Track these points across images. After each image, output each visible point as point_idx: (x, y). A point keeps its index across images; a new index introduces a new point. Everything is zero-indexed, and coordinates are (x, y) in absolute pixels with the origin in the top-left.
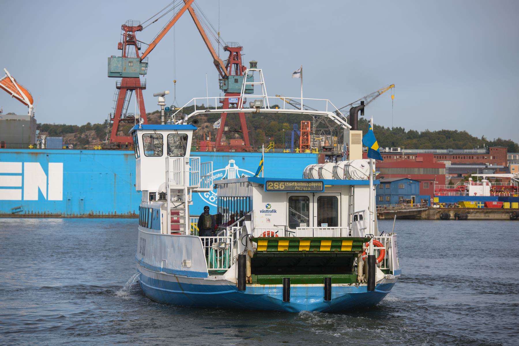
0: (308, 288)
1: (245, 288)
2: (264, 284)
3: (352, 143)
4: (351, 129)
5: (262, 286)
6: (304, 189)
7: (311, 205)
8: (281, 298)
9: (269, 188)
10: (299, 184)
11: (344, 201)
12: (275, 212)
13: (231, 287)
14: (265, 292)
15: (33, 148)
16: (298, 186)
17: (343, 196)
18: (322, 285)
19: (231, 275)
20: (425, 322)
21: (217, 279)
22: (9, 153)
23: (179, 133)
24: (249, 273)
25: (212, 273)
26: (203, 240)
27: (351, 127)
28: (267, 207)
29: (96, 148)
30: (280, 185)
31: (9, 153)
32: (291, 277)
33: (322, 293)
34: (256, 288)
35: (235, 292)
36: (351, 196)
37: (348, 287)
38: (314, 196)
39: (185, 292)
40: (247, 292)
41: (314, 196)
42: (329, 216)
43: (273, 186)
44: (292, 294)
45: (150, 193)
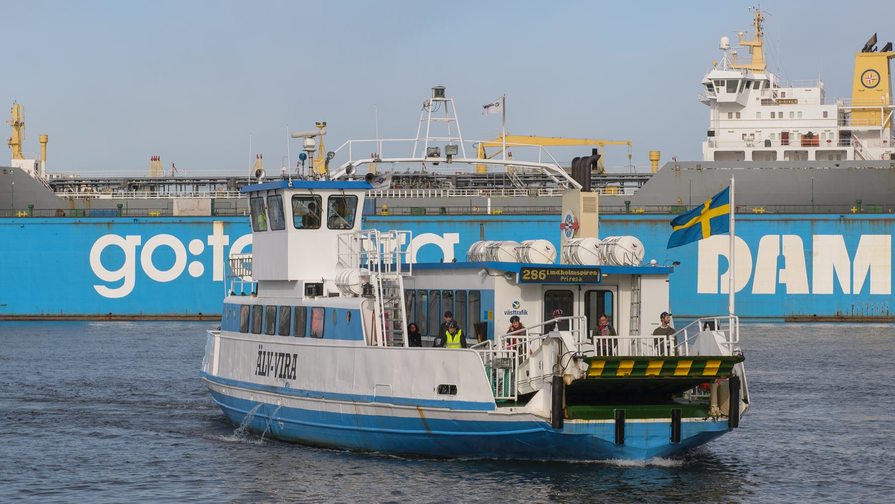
0: (648, 424)
1: (561, 426)
2: (588, 419)
3: (585, 211)
4: (582, 190)
5: (586, 422)
6: (573, 279)
7: (576, 304)
8: (613, 440)
9: (524, 278)
10: (566, 273)
11: (623, 300)
12: (526, 313)
13: (541, 424)
14: (590, 431)
15: (856, 213)
16: (565, 276)
17: (621, 292)
18: (669, 420)
19: (540, 407)
20: (418, 482)
21: (513, 412)
22: (749, 220)
23: (346, 193)
24: (564, 405)
25: (500, 404)
26: (481, 354)
27: (581, 187)
28: (514, 306)
29: (20, 214)
30: (540, 273)
31: (749, 220)
32: (625, 409)
33: (668, 432)
34: (574, 425)
35: (543, 432)
36: (637, 291)
37: (702, 423)
38: (580, 290)
39: (433, 432)
40: (565, 431)
41: (580, 290)
42: (600, 318)
43: (530, 275)
44: (627, 432)
45: (307, 284)
